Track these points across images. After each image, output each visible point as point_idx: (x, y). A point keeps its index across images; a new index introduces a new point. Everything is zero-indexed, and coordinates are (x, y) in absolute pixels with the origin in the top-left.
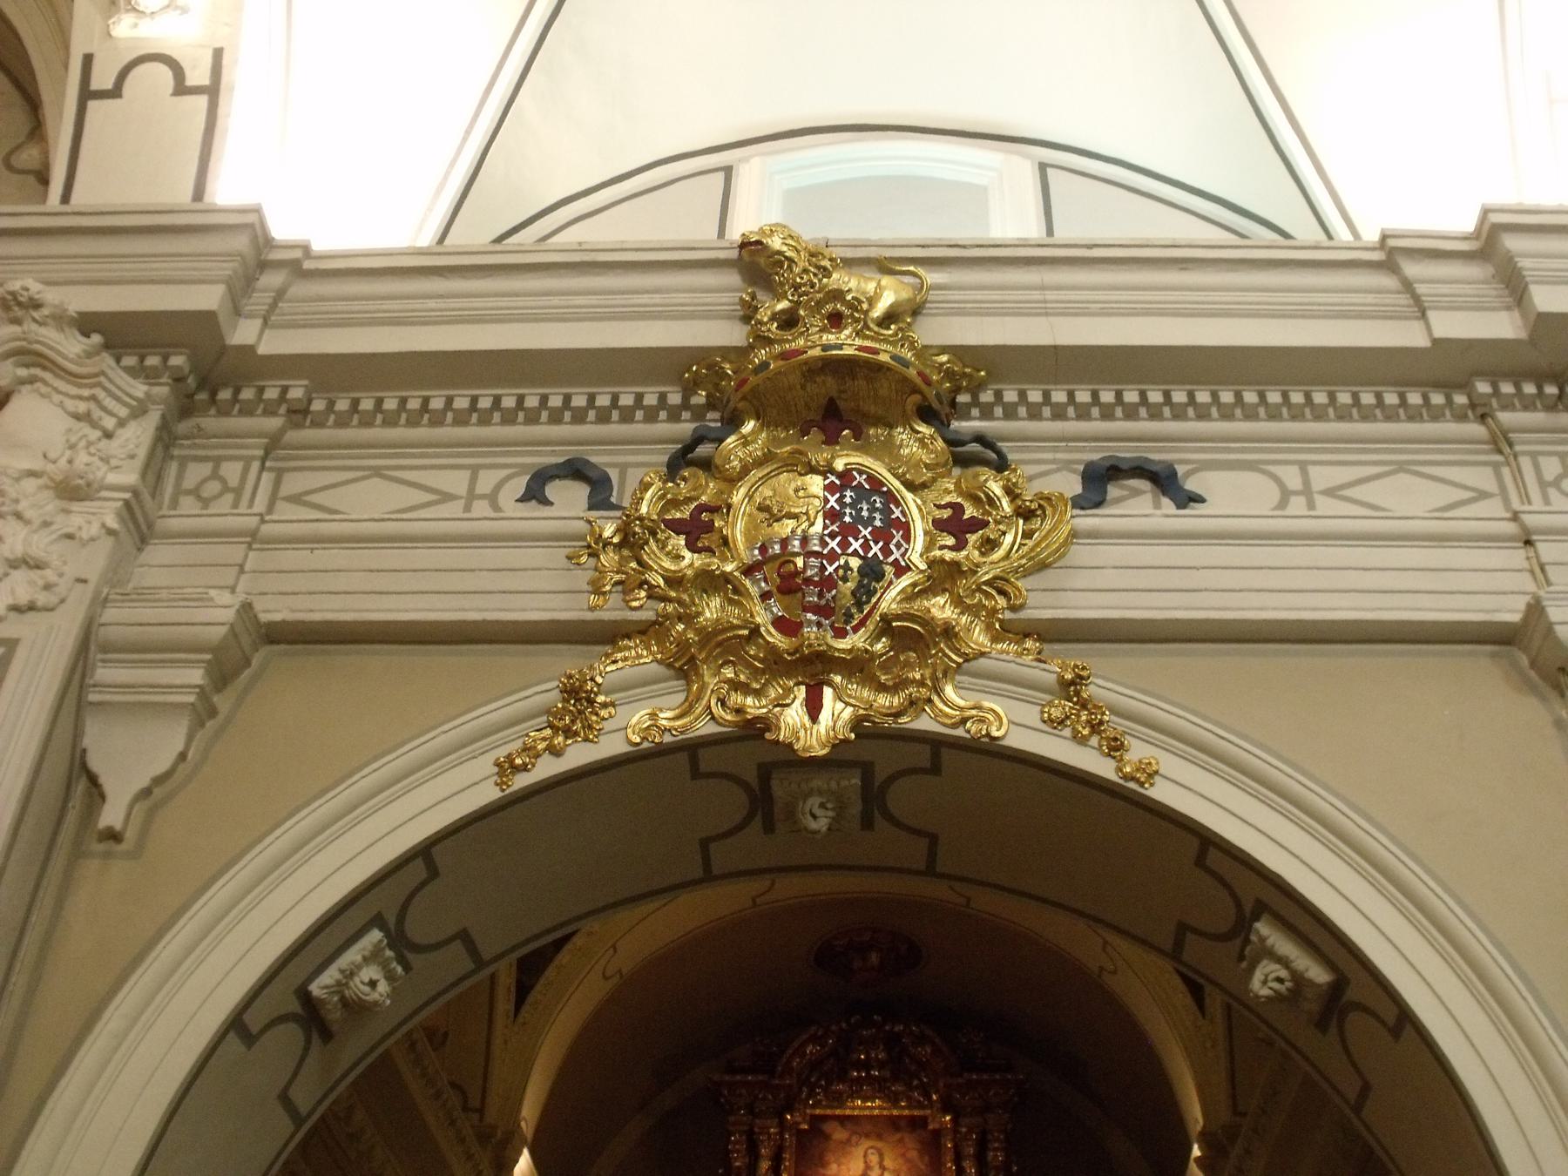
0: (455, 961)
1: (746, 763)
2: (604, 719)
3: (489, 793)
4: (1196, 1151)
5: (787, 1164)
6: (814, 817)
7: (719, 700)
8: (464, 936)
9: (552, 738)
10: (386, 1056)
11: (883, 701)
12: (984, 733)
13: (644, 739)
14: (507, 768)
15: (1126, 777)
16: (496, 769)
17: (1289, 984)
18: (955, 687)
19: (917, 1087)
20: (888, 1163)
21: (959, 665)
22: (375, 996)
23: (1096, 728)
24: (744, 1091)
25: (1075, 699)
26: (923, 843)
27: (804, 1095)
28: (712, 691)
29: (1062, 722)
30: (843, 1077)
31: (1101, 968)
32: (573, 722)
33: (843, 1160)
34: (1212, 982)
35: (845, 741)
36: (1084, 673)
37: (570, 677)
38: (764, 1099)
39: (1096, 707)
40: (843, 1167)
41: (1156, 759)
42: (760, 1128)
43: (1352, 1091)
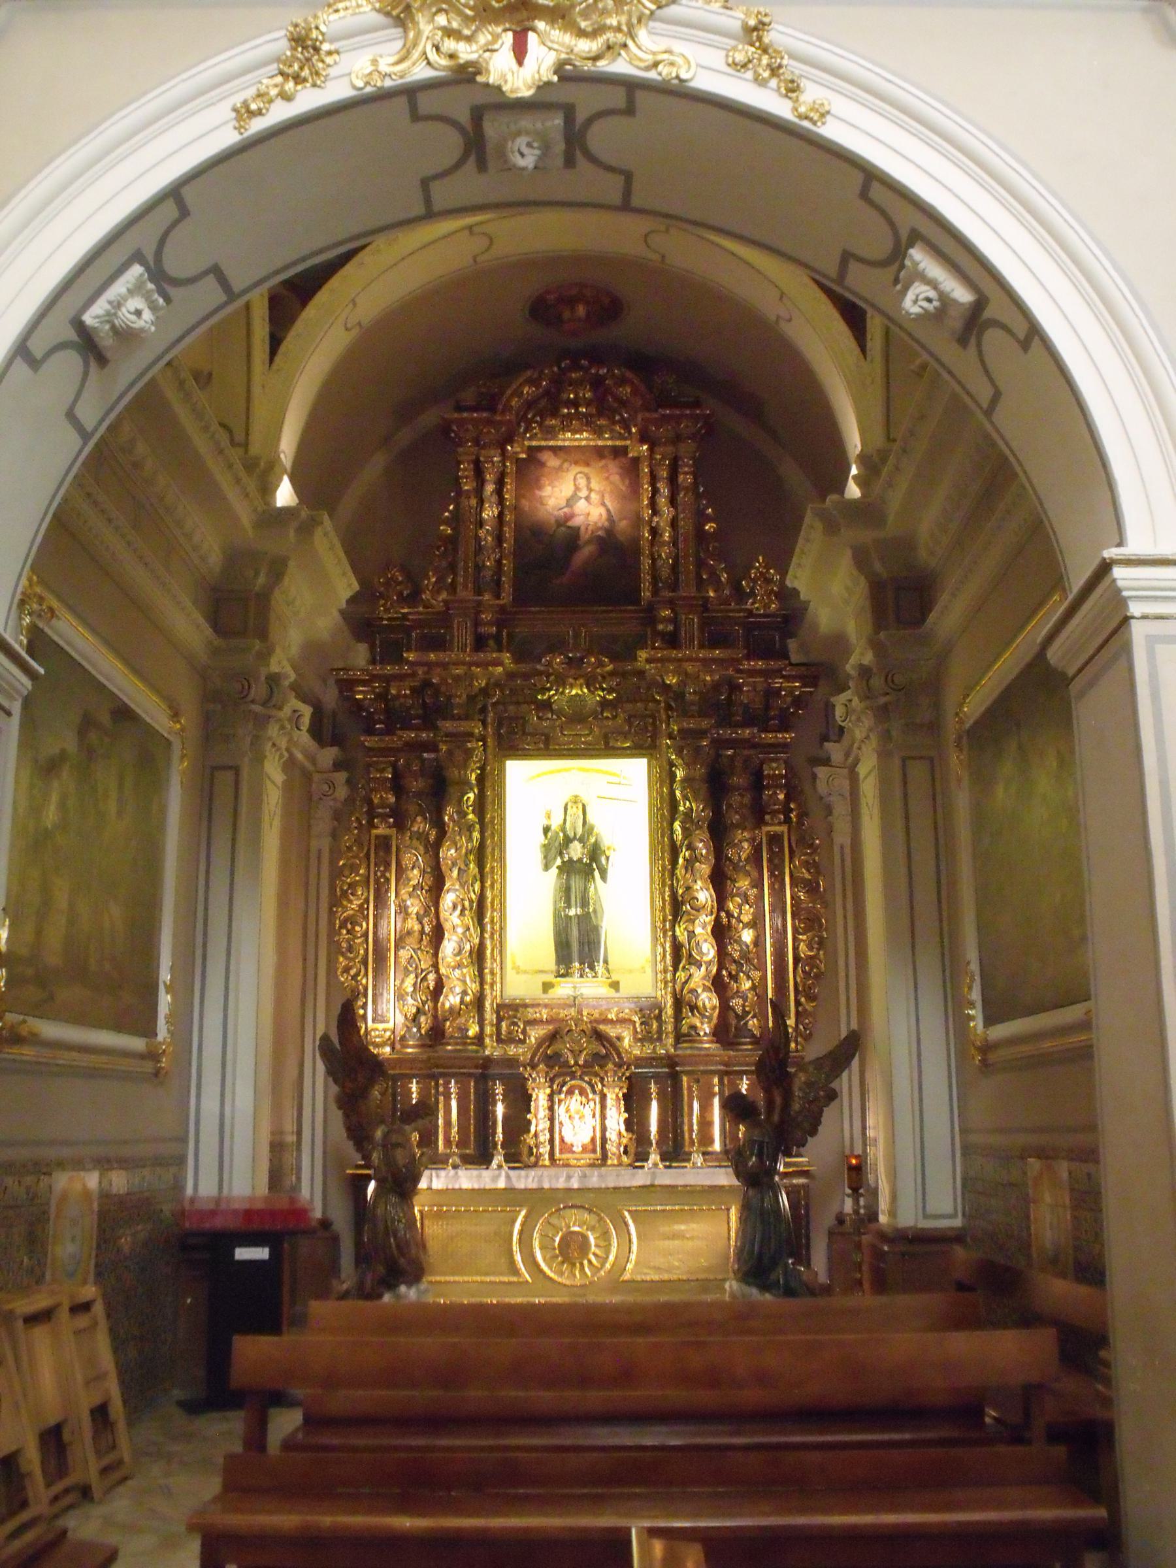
0: (209, 294)
1: (459, 106)
2: (329, 66)
3: (229, 137)
4: (854, 471)
5: (509, 487)
6: (522, 155)
7: (434, 45)
8: (216, 271)
9: (282, 85)
10: (152, 383)
11: (586, 46)
12: (674, 75)
13: (367, 83)
14: (245, 113)
15: (800, 117)
16: (234, 115)
17: (936, 304)
18: (650, 33)
19: (619, 422)
20: (594, 485)
21: (652, 13)
22: (139, 324)
23: (775, 71)
24: (470, 427)
25: (757, 44)
26: (618, 181)
27: (522, 430)
28: (428, 38)
29: (744, 66)
30: (554, 413)
31: (778, 317)
32: (301, 68)
33: (557, 483)
34: (873, 305)
35: (548, 84)
36: (766, 20)
37: (296, 26)
38: (489, 432)
39: (776, 51)
40: (556, 489)
41: (827, 99)
42: (484, 457)
43: (984, 394)
